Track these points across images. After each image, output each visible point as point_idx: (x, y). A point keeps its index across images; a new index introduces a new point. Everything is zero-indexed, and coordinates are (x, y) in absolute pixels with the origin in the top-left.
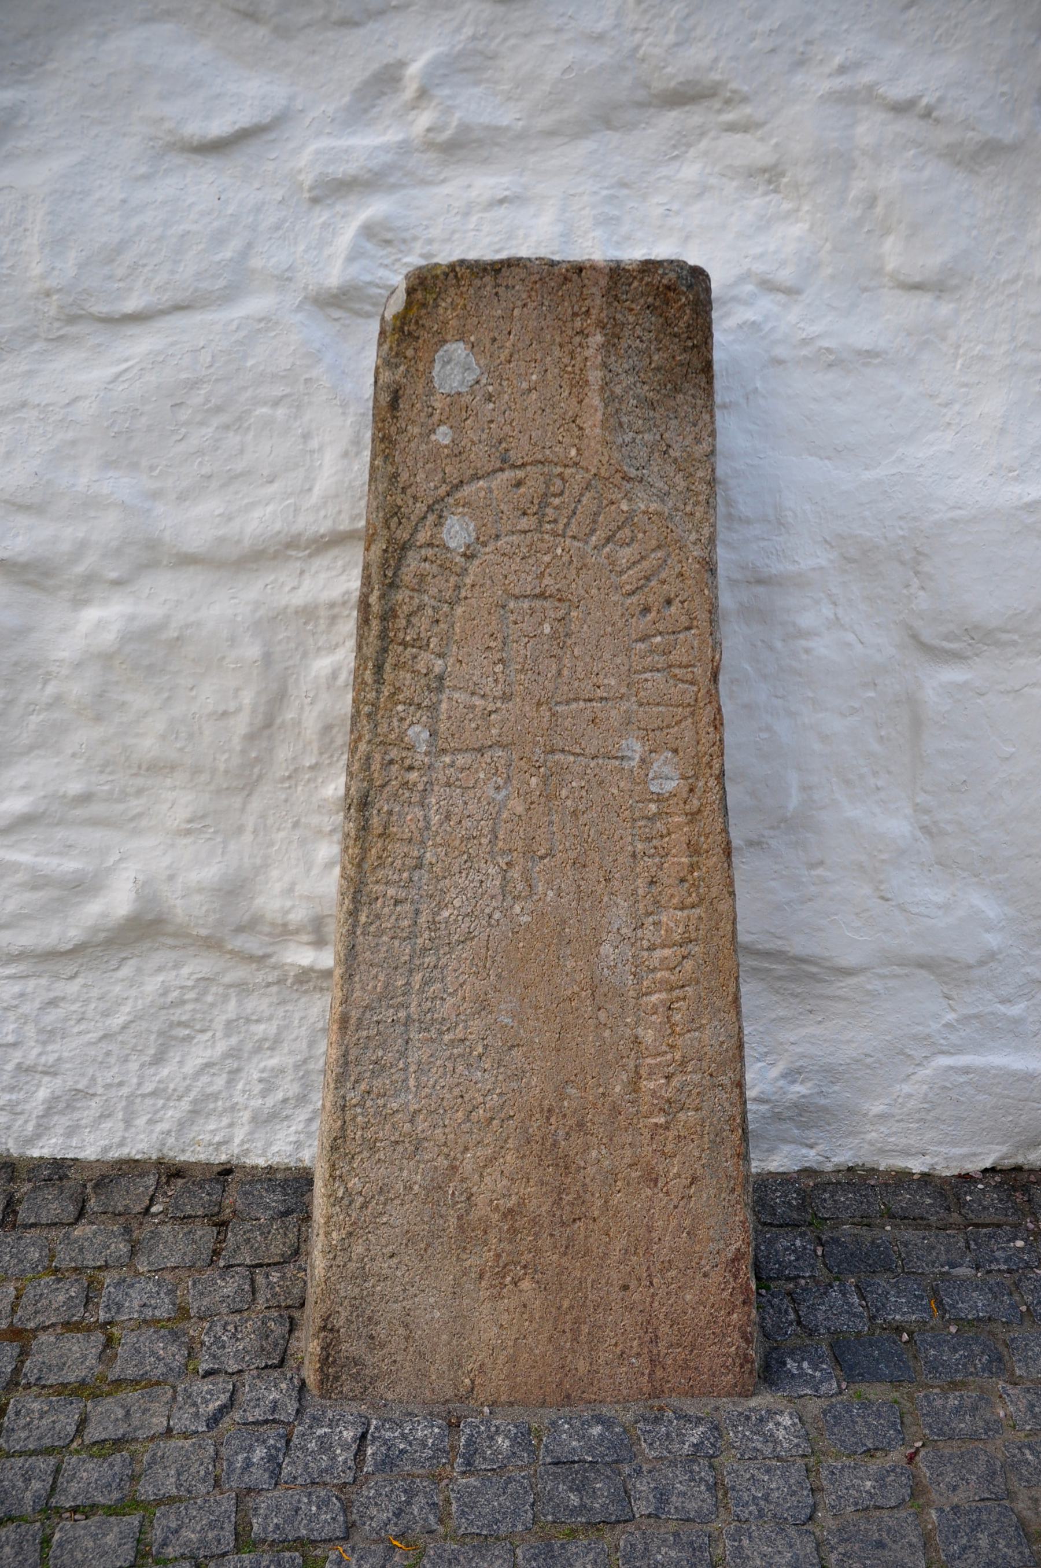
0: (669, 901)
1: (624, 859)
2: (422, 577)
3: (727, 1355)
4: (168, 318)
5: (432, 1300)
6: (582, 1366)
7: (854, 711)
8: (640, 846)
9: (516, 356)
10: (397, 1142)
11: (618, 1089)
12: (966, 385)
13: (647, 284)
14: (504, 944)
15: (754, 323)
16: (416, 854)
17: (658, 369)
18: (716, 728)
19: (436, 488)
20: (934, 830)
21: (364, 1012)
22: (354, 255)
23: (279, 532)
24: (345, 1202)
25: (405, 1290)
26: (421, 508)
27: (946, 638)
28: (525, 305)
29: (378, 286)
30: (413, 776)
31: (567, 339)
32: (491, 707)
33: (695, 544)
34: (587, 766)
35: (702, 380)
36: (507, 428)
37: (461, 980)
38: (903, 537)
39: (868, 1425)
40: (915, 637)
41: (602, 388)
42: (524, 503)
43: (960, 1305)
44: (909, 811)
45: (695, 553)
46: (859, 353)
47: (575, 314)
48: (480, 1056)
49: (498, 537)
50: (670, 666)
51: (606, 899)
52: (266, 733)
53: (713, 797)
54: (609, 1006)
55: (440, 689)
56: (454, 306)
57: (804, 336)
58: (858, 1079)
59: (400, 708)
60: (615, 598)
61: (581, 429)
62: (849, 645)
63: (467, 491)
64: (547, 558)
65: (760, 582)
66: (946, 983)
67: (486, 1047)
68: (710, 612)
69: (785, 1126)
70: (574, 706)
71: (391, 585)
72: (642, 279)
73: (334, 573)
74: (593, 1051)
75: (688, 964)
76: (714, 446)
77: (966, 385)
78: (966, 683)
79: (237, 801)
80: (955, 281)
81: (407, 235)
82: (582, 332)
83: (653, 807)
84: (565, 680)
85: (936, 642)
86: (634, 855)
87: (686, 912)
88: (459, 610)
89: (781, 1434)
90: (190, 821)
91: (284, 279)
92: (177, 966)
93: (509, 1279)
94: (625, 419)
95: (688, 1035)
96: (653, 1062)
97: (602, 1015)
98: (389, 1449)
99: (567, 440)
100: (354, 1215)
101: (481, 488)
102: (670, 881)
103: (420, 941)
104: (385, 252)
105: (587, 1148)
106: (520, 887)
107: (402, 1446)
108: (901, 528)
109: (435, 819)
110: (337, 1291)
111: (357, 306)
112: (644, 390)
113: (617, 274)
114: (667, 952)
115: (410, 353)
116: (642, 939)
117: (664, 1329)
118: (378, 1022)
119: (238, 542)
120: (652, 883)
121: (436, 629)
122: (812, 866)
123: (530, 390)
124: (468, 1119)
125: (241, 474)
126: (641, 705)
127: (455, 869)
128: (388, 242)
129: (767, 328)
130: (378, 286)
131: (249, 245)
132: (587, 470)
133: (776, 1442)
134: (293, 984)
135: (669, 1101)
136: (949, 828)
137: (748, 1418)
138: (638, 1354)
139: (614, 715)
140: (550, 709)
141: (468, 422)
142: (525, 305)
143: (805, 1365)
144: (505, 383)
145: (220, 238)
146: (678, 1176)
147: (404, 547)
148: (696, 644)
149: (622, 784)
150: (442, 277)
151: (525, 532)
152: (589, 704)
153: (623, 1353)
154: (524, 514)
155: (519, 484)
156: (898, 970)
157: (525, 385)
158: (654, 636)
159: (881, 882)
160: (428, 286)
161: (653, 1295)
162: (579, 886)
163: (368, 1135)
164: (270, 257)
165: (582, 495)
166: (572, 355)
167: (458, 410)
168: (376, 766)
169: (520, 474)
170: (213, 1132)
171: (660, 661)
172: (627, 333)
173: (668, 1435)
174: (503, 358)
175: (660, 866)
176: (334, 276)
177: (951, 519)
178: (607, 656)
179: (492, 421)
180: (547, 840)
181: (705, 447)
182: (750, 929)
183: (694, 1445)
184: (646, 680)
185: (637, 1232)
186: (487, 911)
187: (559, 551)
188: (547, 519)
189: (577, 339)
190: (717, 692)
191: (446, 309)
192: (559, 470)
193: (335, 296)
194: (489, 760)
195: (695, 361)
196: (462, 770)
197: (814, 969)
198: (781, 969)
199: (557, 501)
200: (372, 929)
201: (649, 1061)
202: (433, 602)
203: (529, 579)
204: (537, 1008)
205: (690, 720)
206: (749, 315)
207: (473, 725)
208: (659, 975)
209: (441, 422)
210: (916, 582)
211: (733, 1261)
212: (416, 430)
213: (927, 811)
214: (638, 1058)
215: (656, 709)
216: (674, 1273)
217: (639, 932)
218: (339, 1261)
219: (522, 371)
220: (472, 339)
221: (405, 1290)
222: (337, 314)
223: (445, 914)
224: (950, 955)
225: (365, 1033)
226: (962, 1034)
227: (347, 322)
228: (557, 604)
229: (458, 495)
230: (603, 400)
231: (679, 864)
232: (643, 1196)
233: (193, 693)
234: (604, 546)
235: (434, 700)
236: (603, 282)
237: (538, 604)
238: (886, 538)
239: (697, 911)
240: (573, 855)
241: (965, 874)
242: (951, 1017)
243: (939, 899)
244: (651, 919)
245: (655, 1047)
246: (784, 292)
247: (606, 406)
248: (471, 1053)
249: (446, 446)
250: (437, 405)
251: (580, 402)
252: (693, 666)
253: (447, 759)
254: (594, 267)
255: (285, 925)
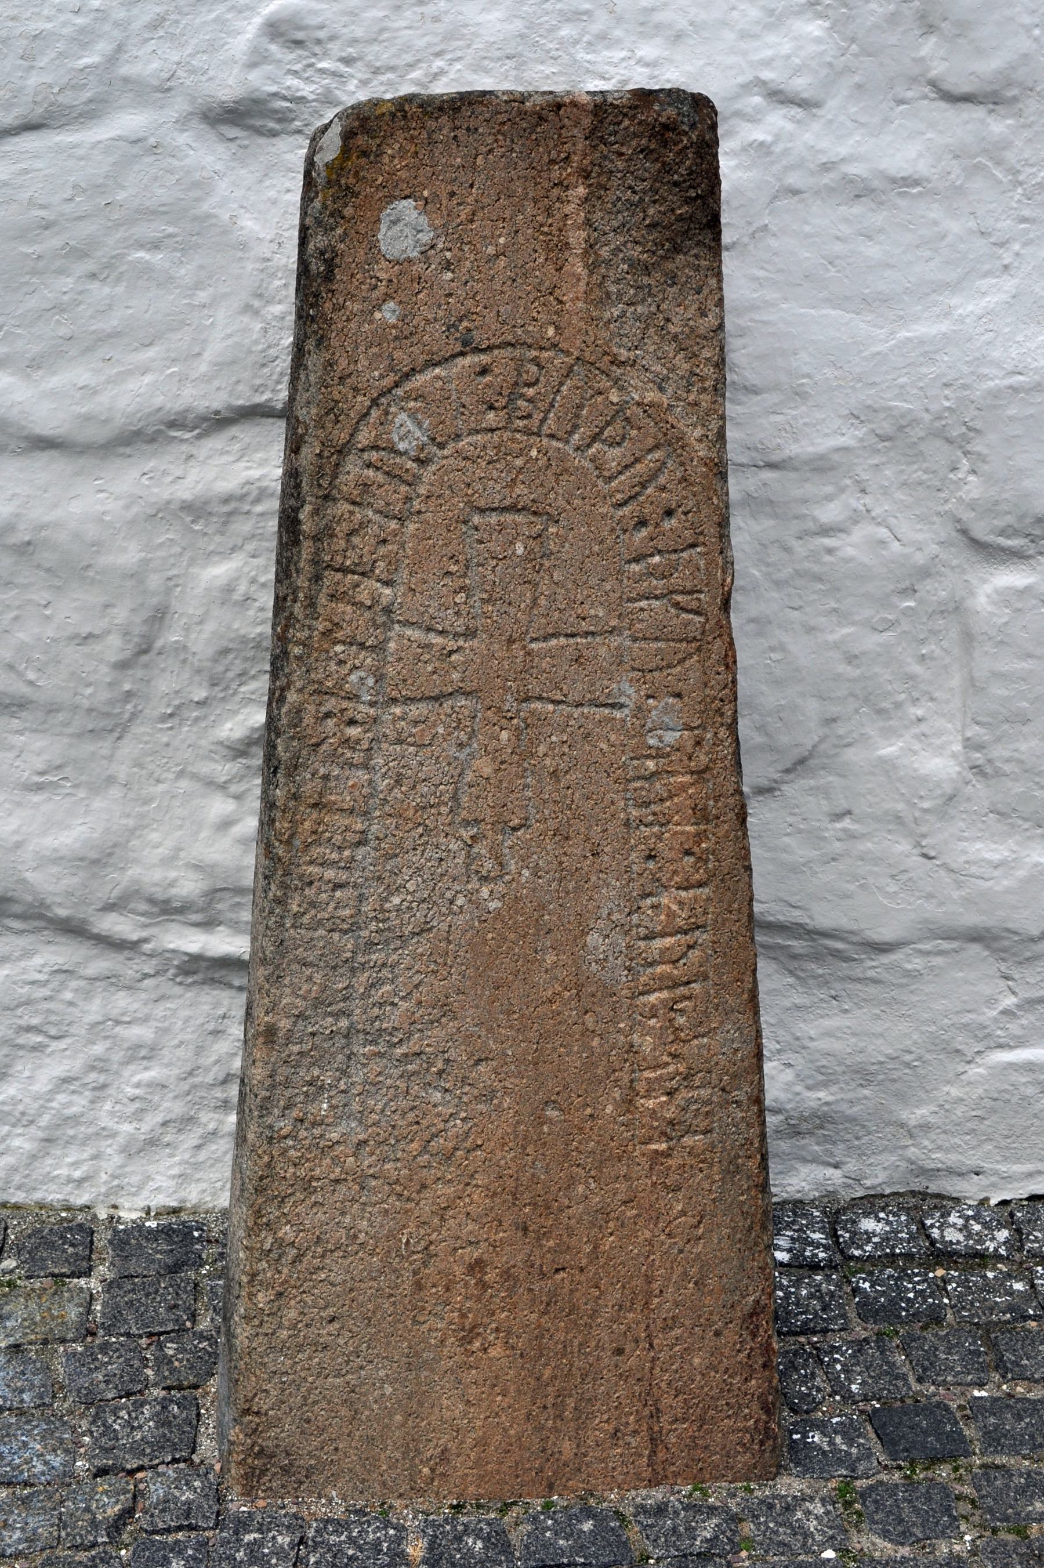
0: (671, 879)
1: (615, 828)
2: (366, 486)
3: (746, 1430)
4: (16, 139)
5: (382, 1373)
6: (567, 1447)
7: (892, 625)
8: (635, 813)
9: (480, 214)
10: (337, 1181)
11: (609, 1109)
12: (1024, 220)
13: (640, 123)
14: (469, 935)
15: (762, 144)
16: (359, 827)
17: (653, 226)
18: (727, 666)
19: (382, 377)
20: (989, 770)
21: (295, 1024)
22: (257, 59)
23: (160, 409)
24: (274, 1255)
25: (347, 1362)
26: (362, 401)
27: (1002, 533)
28: (490, 151)
29: (285, 98)
30: (353, 732)
31: (542, 193)
32: (452, 645)
33: (700, 441)
34: (570, 716)
35: (707, 237)
36: (470, 303)
37: (417, 978)
38: (949, 409)
39: (916, 1510)
40: (964, 532)
41: (586, 252)
42: (490, 395)
43: (1025, 1362)
44: (957, 747)
45: (700, 454)
46: (893, 180)
47: (552, 162)
48: (440, 1073)
49: (458, 436)
50: (671, 592)
51: (594, 878)
52: (145, 658)
53: (726, 750)
54: (598, 1009)
55: (387, 627)
56: (402, 152)
57: (825, 160)
58: (895, 1081)
59: (339, 648)
60: (604, 510)
61: (561, 302)
62: (882, 542)
63: (419, 380)
64: (519, 462)
65: (771, 466)
66: (1003, 960)
67: (447, 1061)
68: (720, 525)
69: (803, 1142)
70: (553, 642)
71: (326, 497)
72: (634, 117)
73: (231, 459)
74: (578, 1064)
75: (694, 955)
76: (722, 318)
77: (1024, 220)
78: (1028, 589)
79: (104, 747)
80: (1010, 93)
81: (322, 34)
82: (560, 183)
83: (651, 764)
84: (542, 610)
85: (991, 538)
86: (627, 824)
87: (691, 892)
88: (412, 527)
89: (812, 1525)
90: (42, 773)
91: (164, 89)
92: (27, 954)
93: (477, 1344)
94: (613, 289)
95: (696, 1042)
96: (652, 1075)
97: (589, 1019)
98: (335, 1557)
99: (543, 317)
100: (285, 1271)
101: (438, 378)
102: (672, 855)
103: (365, 933)
104: (292, 56)
105: (572, 1181)
106: (488, 865)
107: (350, 1552)
108: (947, 398)
109: (383, 784)
110: (264, 1365)
111: (258, 123)
112: (635, 252)
113: (604, 112)
114: (669, 941)
115: (348, 211)
116: (638, 926)
117: (667, 1401)
118: (313, 1034)
119: (106, 421)
120: (650, 857)
121: (382, 550)
122: (838, 817)
123: (497, 256)
124: (424, 1150)
125: (110, 336)
126: (635, 640)
127: (408, 844)
128: (298, 43)
129: (778, 149)
130: (285, 98)
131: (120, 48)
132: (568, 353)
133: (807, 1534)
134: (176, 976)
135: (671, 1123)
136: (1007, 768)
137: (771, 1507)
138: (636, 1432)
139: (603, 649)
140: (524, 647)
141: (420, 296)
142: (490, 151)
143: (838, 1440)
144: (466, 248)
145: (83, 39)
146: (683, 1213)
147: (342, 452)
148: (702, 563)
149: (613, 737)
150: (387, 118)
151: (492, 430)
152: (572, 641)
153: (617, 1430)
154: (491, 407)
155: (484, 371)
156: (946, 945)
157: (491, 250)
158: (652, 555)
159: (924, 836)
160: (365, 126)
161: (654, 1360)
162: (561, 863)
163: (302, 1172)
164: (148, 62)
165: (561, 384)
166: (549, 212)
167: (406, 280)
168: (308, 720)
169: (485, 358)
170: (76, 1164)
171: (658, 585)
172: (615, 182)
173: (674, 1529)
174: (463, 217)
175: (659, 837)
176: (229, 85)
177: (1010, 387)
178: (593, 581)
179: (450, 295)
180: (522, 807)
181: (711, 320)
182: (766, 904)
183: (707, 1541)
184: (642, 609)
185: (634, 1283)
186: (448, 895)
187: (534, 453)
188: (519, 414)
189: (556, 191)
190: (729, 622)
191: (393, 157)
192: (535, 353)
193: (230, 111)
194: (449, 711)
195: (699, 215)
196: (416, 723)
197: (839, 945)
198: (797, 945)
199: (531, 392)
200: (306, 919)
201: (647, 1074)
202: (377, 518)
203: (498, 487)
204: (509, 1013)
205: (696, 658)
206: (759, 134)
207: (430, 669)
208: (659, 969)
209: (387, 297)
210: (965, 464)
211: (751, 1315)
212: (357, 307)
213: (980, 747)
214: (633, 1071)
215: (655, 645)
216: (678, 1332)
217: (635, 917)
218: (267, 1328)
219: (487, 232)
220: (426, 193)
221: (347, 1362)
222: (232, 132)
223: (396, 900)
224: (1010, 925)
225: (296, 1048)
226: (1024, 1022)
227: (246, 142)
228: (533, 519)
229: (408, 386)
230: (586, 266)
231: (682, 833)
232: (641, 1239)
233: (48, 612)
234: (589, 446)
235: (381, 638)
236: (587, 121)
237: (509, 518)
238: (927, 410)
239: (706, 891)
240: (552, 824)
241: (1026, 825)
242: (1010, 1001)
243: (996, 857)
244: (649, 901)
245: (655, 1058)
246: (800, 106)
247: (591, 273)
248: (427, 1070)
249: (394, 327)
250: (382, 275)
251: (559, 270)
252: (700, 592)
253: (398, 710)
254: (574, 104)
255: (167, 902)
